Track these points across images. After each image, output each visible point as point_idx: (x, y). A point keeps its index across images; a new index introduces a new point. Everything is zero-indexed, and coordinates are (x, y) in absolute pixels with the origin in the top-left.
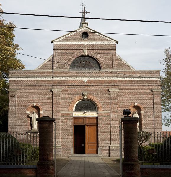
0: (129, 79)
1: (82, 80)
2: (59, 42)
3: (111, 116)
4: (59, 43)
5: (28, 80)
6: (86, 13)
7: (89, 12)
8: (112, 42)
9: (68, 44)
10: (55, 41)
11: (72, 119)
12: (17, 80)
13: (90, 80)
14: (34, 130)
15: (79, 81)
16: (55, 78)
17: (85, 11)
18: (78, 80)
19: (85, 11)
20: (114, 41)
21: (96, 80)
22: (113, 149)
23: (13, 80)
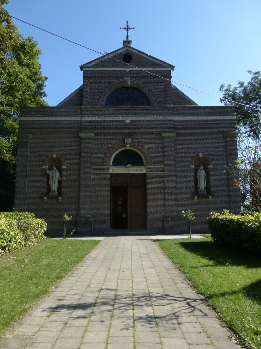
8: (166, 67)
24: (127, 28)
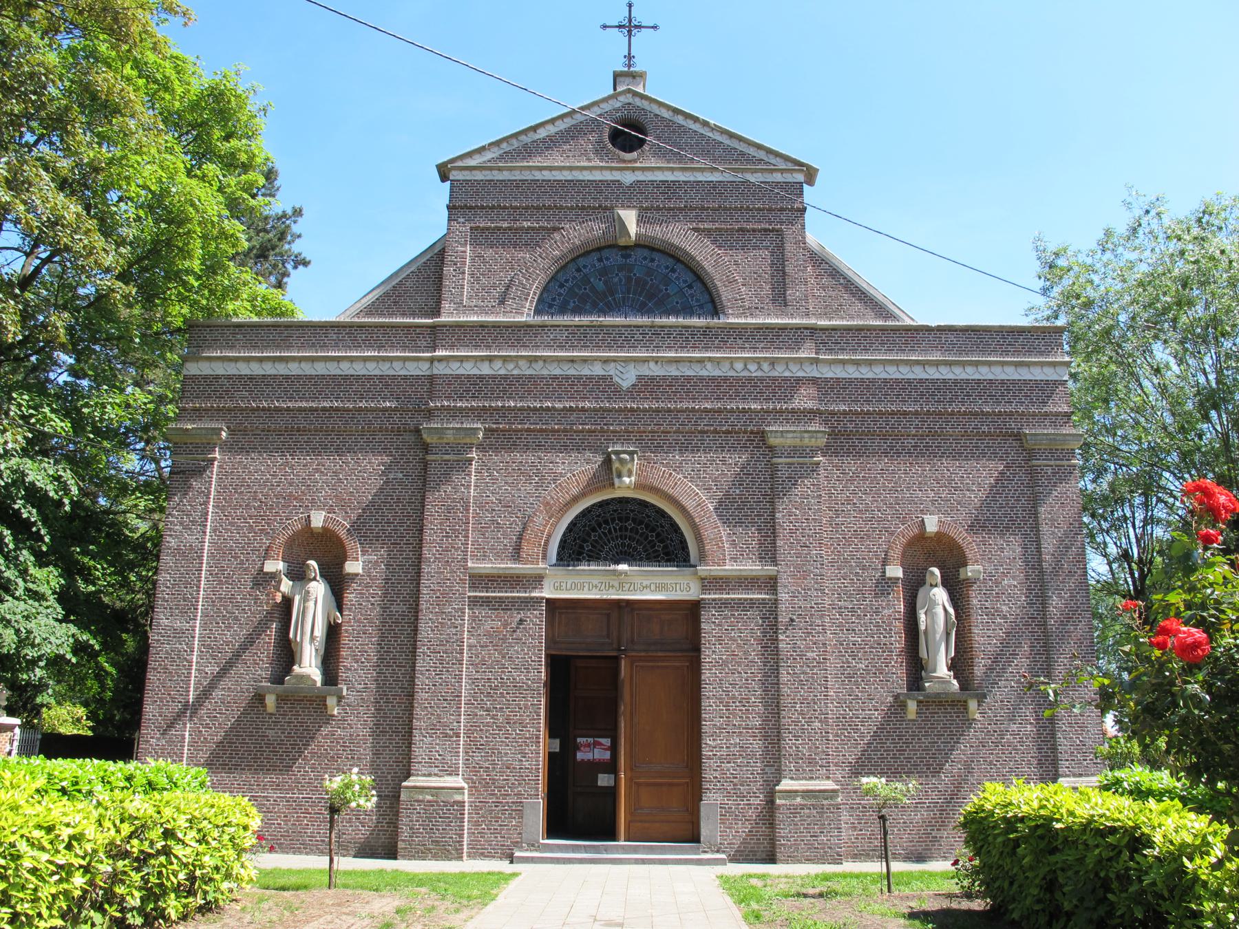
0: (884, 376)
1: (604, 378)
2: (491, 169)
3: (783, 596)
4: (479, 176)
5: (287, 377)
6: (634, 31)
7: (655, 27)
8: (782, 171)
9: (692, 179)
10: (459, 164)
11: (537, 621)
12: (229, 377)
13: (652, 378)
14: (302, 678)
15: (585, 385)
16: (444, 364)
17: (630, 21)
18: (579, 378)
19: (630, 21)
20: (790, 166)
21: (688, 379)
22: (795, 810)
23: (205, 377)
24: (630, 27)
